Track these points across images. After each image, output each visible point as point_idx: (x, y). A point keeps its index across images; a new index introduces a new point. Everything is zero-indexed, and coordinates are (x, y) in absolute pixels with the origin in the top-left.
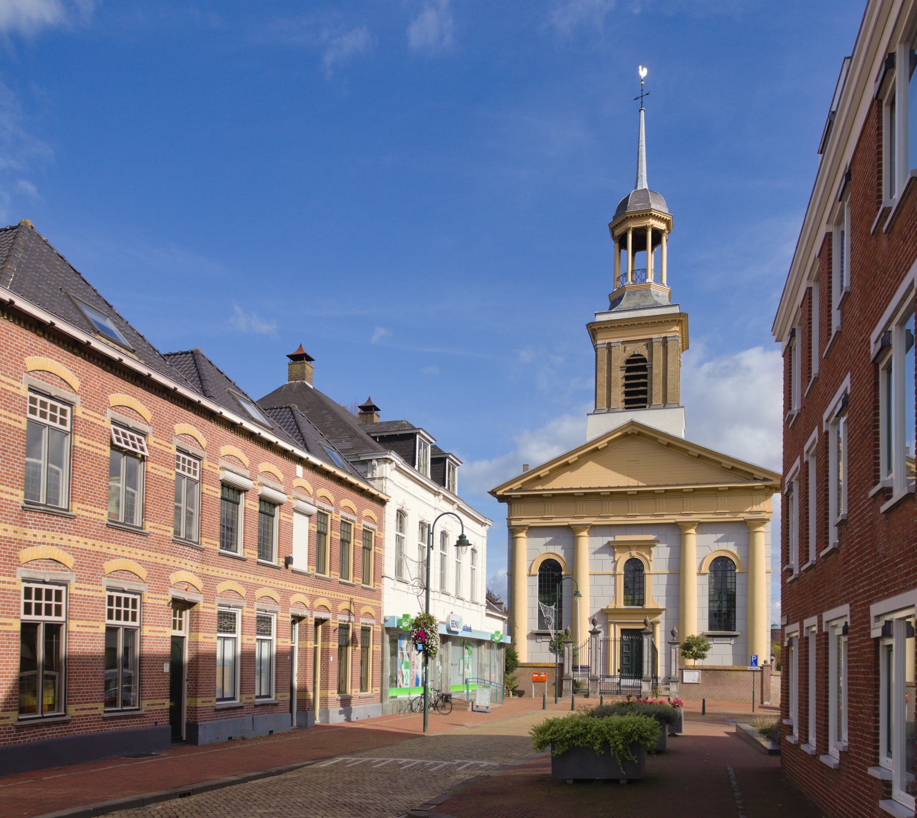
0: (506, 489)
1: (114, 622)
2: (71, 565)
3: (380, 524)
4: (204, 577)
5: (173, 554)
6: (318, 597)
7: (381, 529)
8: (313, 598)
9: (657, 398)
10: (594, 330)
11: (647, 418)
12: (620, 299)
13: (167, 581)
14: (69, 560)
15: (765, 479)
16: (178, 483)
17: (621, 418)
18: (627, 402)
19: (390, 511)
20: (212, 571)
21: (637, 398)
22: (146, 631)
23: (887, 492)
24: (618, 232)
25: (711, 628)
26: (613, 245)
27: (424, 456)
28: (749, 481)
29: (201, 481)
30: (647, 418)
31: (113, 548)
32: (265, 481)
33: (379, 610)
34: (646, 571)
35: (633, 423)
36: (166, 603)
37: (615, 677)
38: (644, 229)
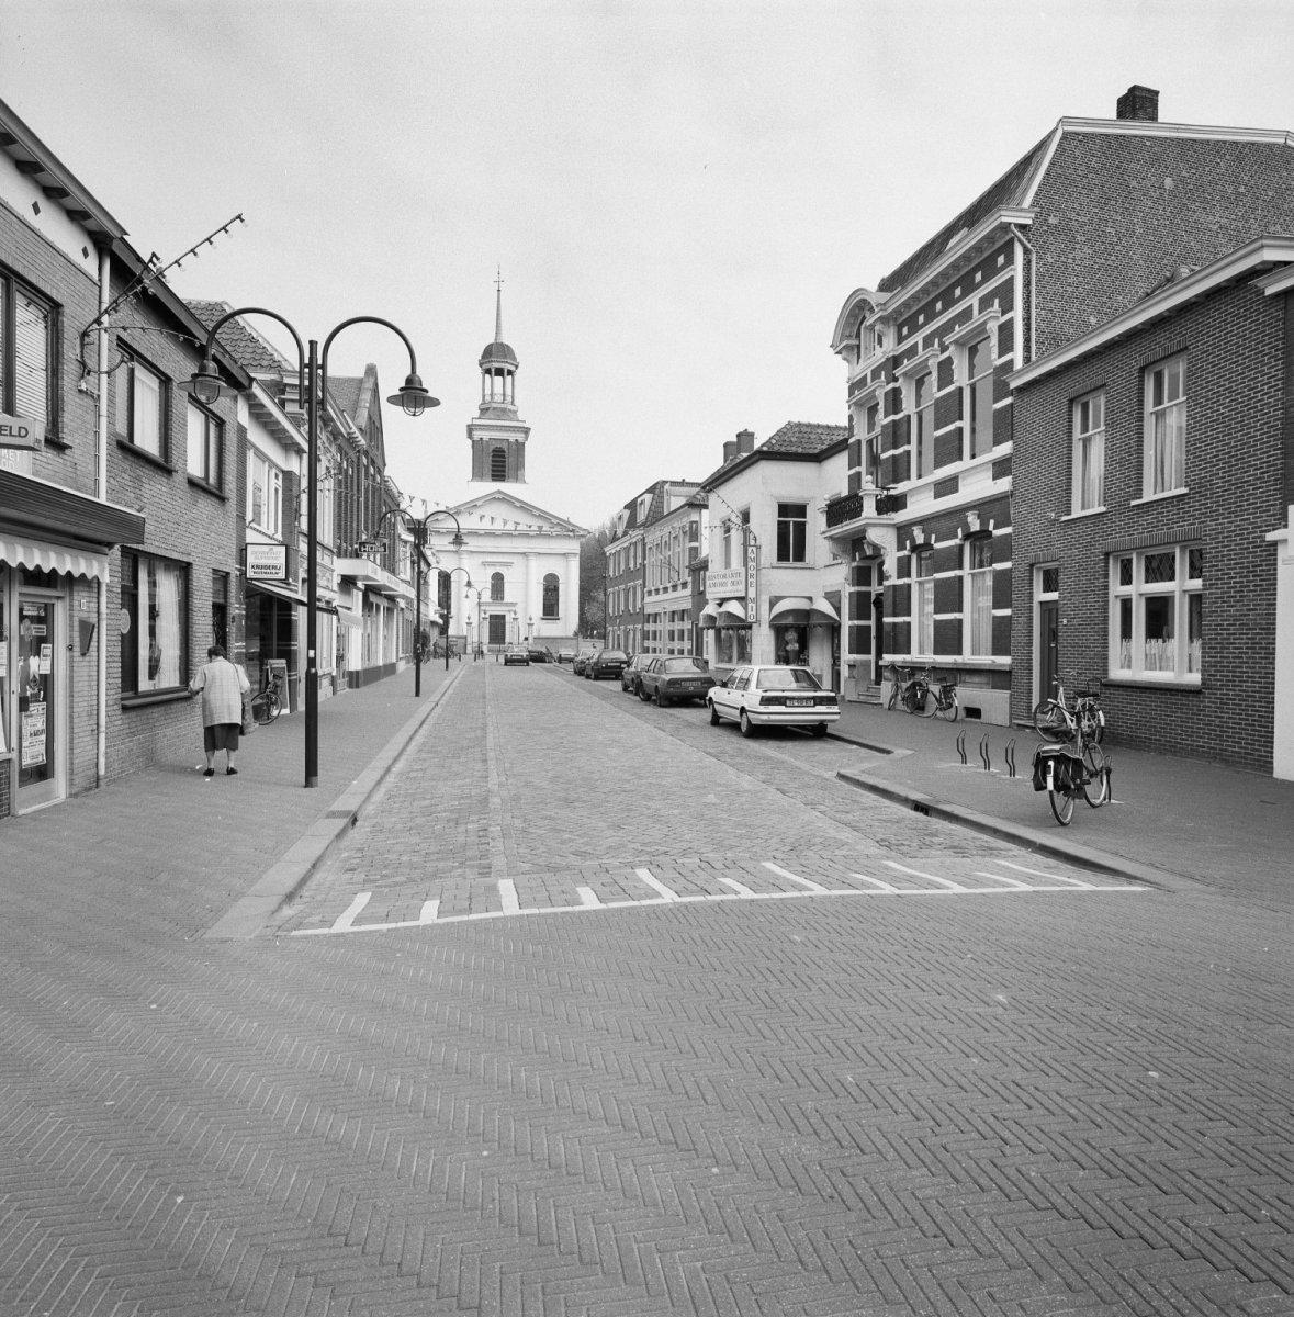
18: (493, 476)
30: (507, 487)
35: (500, 492)
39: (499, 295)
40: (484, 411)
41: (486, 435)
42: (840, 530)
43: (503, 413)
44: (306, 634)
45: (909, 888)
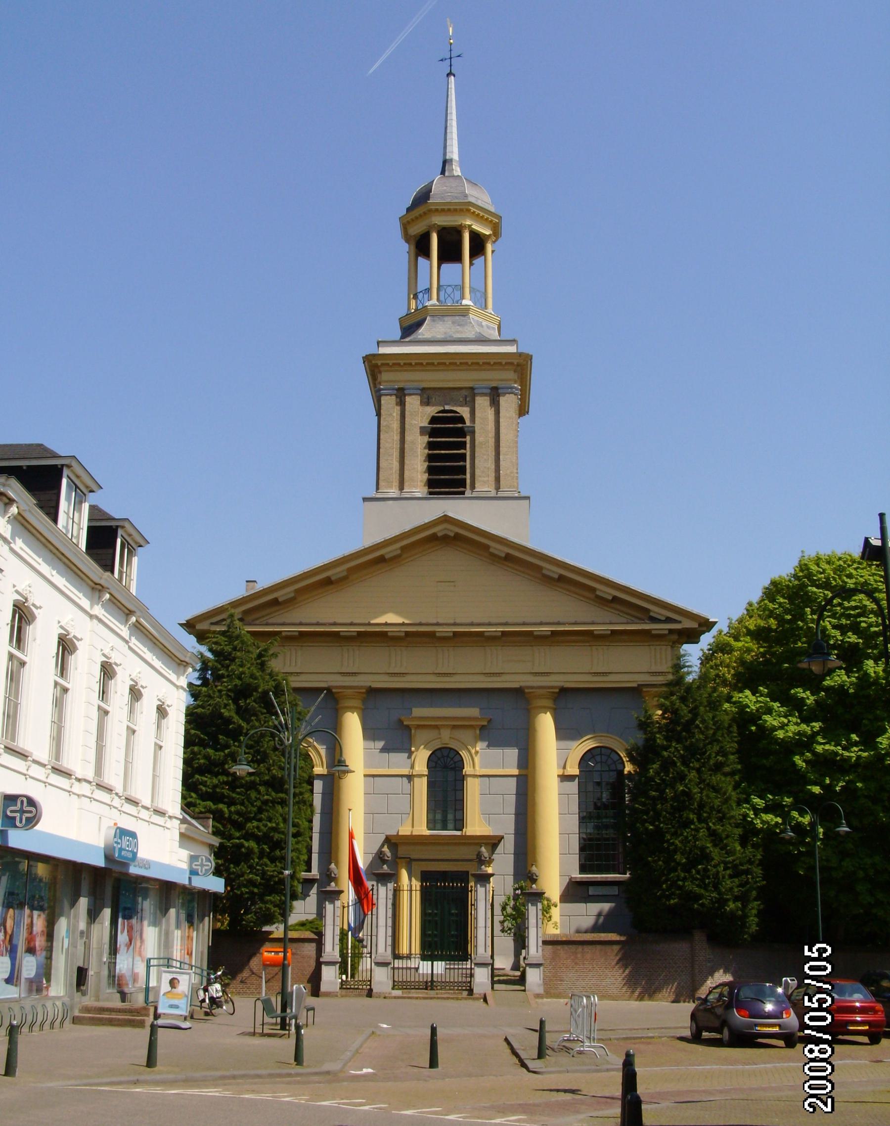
0: (214, 620)
9: (484, 484)
10: (376, 366)
11: (462, 510)
12: (420, 324)
15: (669, 620)
18: (431, 484)
24: (416, 229)
25: (583, 869)
26: (403, 249)
27: (73, 522)
28: (641, 620)
30: (462, 510)
34: (467, 769)
37: (409, 957)
38: (457, 232)
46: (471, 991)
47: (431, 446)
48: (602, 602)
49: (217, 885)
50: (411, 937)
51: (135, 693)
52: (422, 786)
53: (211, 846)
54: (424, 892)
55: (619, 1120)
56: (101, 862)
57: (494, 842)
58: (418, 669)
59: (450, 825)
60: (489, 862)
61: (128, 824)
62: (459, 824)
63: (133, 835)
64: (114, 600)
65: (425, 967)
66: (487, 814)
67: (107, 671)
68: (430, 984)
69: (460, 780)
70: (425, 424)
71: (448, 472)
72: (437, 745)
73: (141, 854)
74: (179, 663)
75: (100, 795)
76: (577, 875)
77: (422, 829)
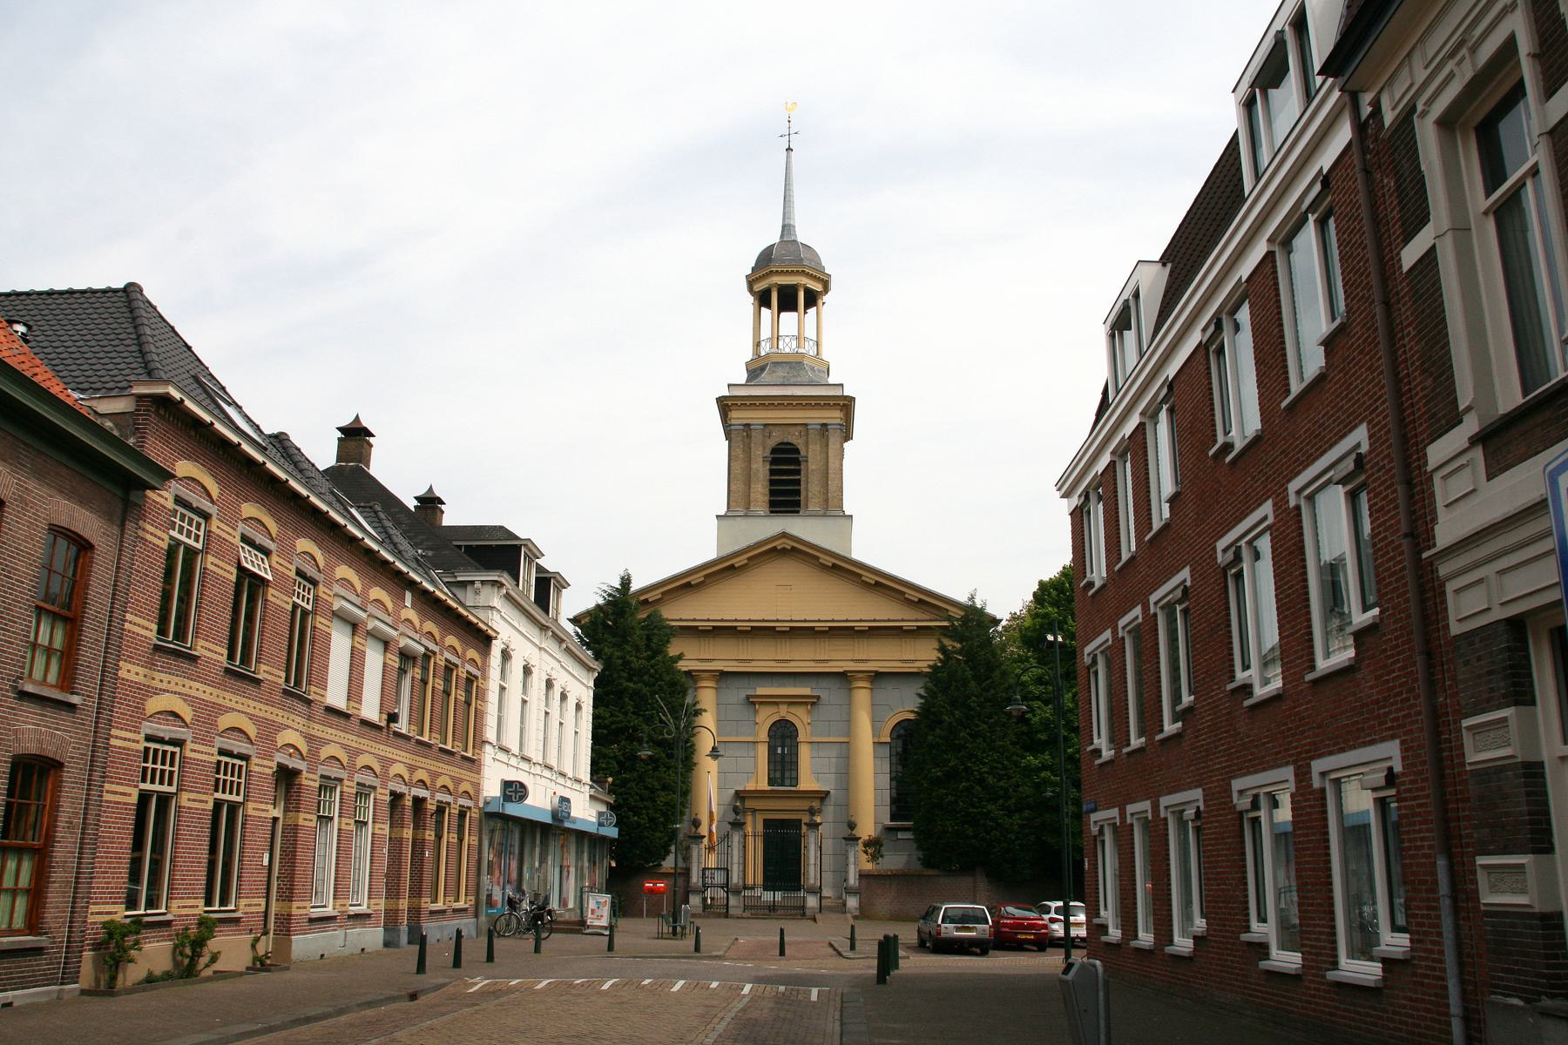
1: (147, 786)
2: (188, 720)
3: (484, 669)
4: (309, 738)
5: (282, 707)
6: (361, 752)
7: (485, 677)
8: (412, 769)
11: (801, 528)
13: (140, 708)
14: (187, 713)
16: (293, 613)
17: (768, 527)
18: (772, 504)
19: (496, 648)
20: (318, 730)
21: (785, 498)
22: (185, 799)
23: (1228, 447)
24: (758, 287)
27: (527, 577)
29: (314, 612)
30: (801, 528)
31: (161, 679)
32: (343, 592)
33: (477, 787)
35: (784, 535)
36: (269, 771)
39: (788, 157)
40: (755, 370)
41: (757, 417)
42: (812, 861)
43: (794, 364)
44: (957, 958)
45: (199, 404)
46: (804, 914)
47: (772, 472)
48: (909, 603)
49: (613, 832)
50: (755, 874)
51: (564, 697)
52: (763, 751)
53: (608, 804)
54: (766, 837)
55: (875, 962)
56: (549, 820)
57: (823, 796)
58: (763, 657)
59: (787, 782)
60: (820, 811)
61: (567, 794)
62: (795, 781)
63: (568, 800)
64: (555, 635)
65: (768, 896)
66: (817, 774)
67: (549, 684)
68: (772, 908)
69: (795, 747)
70: (767, 453)
71: (785, 498)
72: (776, 718)
73: (573, 814)
74: (590, 669)
75: (547, 773)
76: (888, 822)
77: (764, 785)
